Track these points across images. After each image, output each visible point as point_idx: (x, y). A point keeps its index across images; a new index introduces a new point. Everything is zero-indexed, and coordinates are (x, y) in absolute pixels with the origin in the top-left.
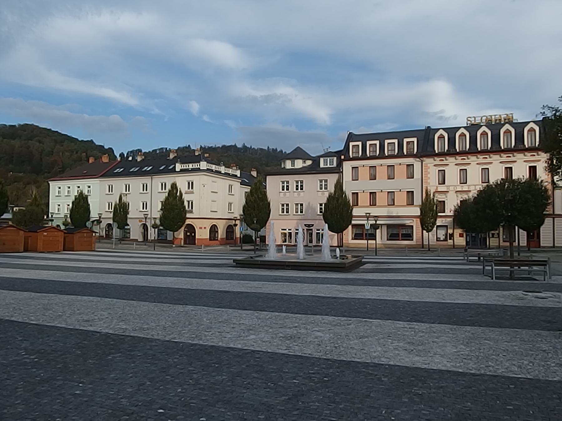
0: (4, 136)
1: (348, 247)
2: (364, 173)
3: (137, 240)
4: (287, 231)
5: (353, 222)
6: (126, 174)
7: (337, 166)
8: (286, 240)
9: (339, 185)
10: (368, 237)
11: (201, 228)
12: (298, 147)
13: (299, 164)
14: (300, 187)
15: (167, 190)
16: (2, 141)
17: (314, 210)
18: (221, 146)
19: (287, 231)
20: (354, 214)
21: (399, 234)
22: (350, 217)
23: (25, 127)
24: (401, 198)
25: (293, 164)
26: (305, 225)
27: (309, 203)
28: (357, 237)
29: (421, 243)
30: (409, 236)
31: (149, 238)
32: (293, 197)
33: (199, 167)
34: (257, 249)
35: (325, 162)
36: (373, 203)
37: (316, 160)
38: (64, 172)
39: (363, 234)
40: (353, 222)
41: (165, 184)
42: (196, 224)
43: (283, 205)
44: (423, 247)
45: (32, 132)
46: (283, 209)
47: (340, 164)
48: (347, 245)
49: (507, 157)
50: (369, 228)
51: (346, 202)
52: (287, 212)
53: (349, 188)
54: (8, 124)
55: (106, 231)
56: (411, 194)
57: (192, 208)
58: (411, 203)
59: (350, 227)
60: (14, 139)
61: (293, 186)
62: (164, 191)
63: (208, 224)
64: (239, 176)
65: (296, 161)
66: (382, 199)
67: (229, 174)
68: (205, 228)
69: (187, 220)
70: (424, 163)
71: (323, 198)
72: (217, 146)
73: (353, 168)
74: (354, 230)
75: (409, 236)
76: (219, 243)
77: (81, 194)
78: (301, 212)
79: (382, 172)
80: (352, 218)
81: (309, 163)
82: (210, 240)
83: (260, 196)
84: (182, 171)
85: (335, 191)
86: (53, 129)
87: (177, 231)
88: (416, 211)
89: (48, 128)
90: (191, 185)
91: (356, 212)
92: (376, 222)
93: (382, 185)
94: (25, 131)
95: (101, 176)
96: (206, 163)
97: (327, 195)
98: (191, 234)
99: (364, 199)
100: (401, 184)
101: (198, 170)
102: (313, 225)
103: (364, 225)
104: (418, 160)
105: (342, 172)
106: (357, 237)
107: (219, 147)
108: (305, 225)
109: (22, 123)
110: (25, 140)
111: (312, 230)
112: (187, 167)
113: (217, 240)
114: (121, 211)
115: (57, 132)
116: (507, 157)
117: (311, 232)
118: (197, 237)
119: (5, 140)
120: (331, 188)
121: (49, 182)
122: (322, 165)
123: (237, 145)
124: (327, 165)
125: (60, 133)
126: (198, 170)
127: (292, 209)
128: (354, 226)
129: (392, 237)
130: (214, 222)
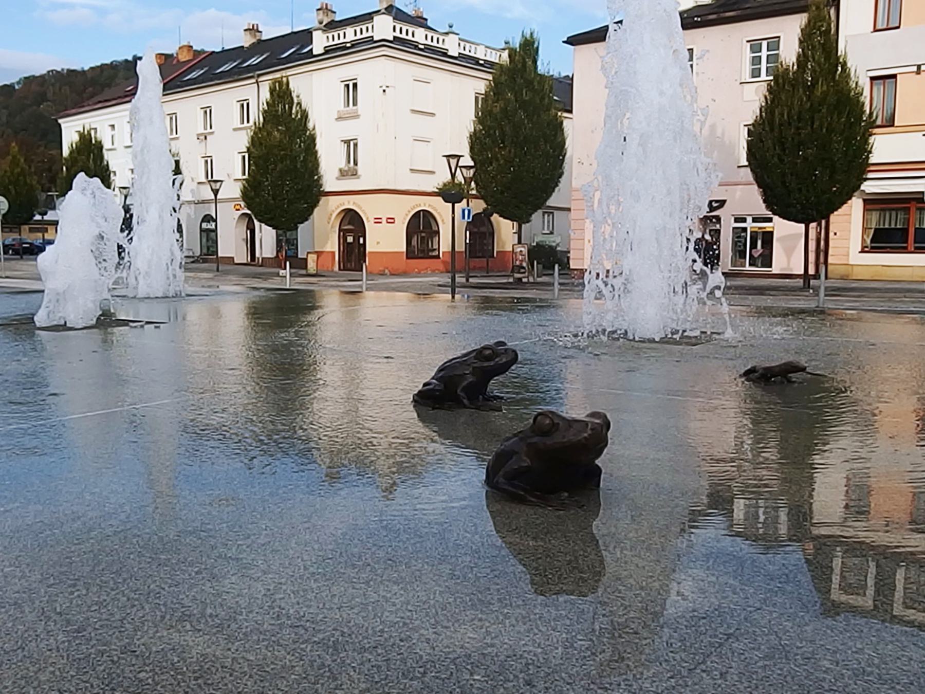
1: (843, 278)
5: (869, 187)
9: (821, 43)
11: (378, 221)
15: (251, 122)
22: (856, 165)
28: (882, 240)
31: (257, 255)
33: (370, 34)
39: (905, 231)
41: (248, 104)
42: (367, 208)
48: (842, 270)
57: (356, 164)
59: (856, 205)
62: (246, 124)
63: (404, 209)
67: (476, 61)
68: (391, 221)
72: (563, 75)
74: (875, 216)
76: (441, 267)
80: (865, 172)
84: (331, 52)
85: (802, 60)
90: (351, 88)
91: (884, 147)
97: (763, 88)
98: (356, 239)
106: (882, 240)
112: (342, 40)
113: (438, 257)
118: (368, 250)
120: (789, 53)
121: (60, 121)
126: (370, 42)
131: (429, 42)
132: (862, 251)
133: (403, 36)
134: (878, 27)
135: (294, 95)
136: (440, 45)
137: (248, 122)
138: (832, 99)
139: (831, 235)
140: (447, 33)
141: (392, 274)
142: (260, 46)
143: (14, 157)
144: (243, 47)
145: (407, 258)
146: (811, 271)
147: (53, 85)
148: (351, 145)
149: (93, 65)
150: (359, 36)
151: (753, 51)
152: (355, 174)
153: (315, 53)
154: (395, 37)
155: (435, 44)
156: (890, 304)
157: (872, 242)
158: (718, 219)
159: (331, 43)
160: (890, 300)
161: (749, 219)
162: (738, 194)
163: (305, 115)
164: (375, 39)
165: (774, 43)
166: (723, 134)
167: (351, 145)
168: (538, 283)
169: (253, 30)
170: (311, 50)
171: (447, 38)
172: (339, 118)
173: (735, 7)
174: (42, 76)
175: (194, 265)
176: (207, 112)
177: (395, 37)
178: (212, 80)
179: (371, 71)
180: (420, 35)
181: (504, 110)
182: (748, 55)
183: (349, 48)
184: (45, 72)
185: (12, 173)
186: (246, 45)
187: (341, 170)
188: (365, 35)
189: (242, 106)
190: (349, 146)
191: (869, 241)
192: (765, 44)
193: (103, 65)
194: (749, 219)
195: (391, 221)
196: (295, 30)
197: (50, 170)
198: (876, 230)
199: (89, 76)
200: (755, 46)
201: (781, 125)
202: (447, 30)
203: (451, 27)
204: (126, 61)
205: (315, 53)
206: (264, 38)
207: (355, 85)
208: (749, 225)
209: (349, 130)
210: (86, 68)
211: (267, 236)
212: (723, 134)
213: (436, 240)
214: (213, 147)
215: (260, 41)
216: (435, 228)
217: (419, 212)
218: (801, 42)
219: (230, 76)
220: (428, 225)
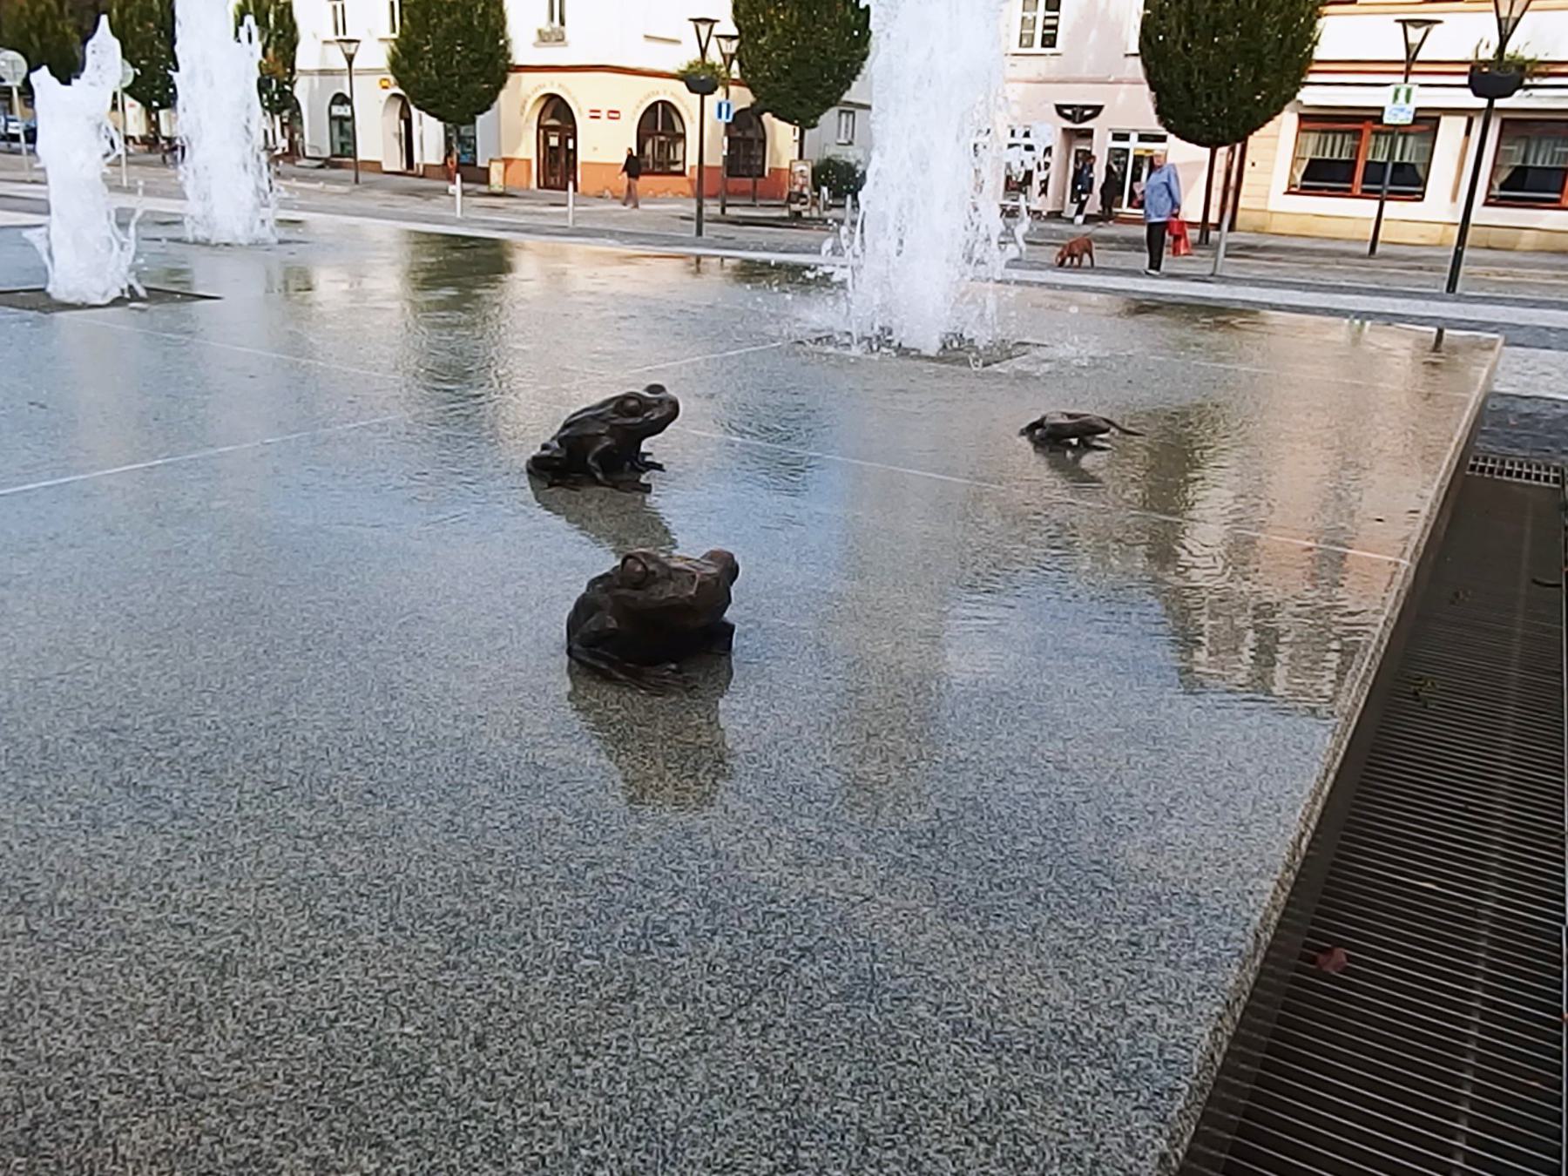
1: (1258, 231)
3: (379, 163)
39: (1352, 164)
42: (579, 93)
48: (1256, 219)
49: (751, 272)
57: (562, 23)
59: (1286, 123)
63: (635, 97)
68: (614, 114)
69: (1308, 89)
74: (1312, 139)
92: (1491, 104)
102: (1098, 109)
106: (1321, 177)
108: (1060, 109)
111: (1089, 134)
113: (682, 173)
116: (751, 272)
128: (1311, 120)
139: (1247, 164)
157: (1304, 178)
158: (1089, 134)
160: (1317, 267)
161: (1134, 137)
162: (1121, 97)
191: (1299, 177)
194: (1134, 137)
195: (614, 114)
198: (1312, 161)
208: (1133, 145)
213: (680, 147)
216: (679, 129)
217: (655, 104)
220: (668, 123)
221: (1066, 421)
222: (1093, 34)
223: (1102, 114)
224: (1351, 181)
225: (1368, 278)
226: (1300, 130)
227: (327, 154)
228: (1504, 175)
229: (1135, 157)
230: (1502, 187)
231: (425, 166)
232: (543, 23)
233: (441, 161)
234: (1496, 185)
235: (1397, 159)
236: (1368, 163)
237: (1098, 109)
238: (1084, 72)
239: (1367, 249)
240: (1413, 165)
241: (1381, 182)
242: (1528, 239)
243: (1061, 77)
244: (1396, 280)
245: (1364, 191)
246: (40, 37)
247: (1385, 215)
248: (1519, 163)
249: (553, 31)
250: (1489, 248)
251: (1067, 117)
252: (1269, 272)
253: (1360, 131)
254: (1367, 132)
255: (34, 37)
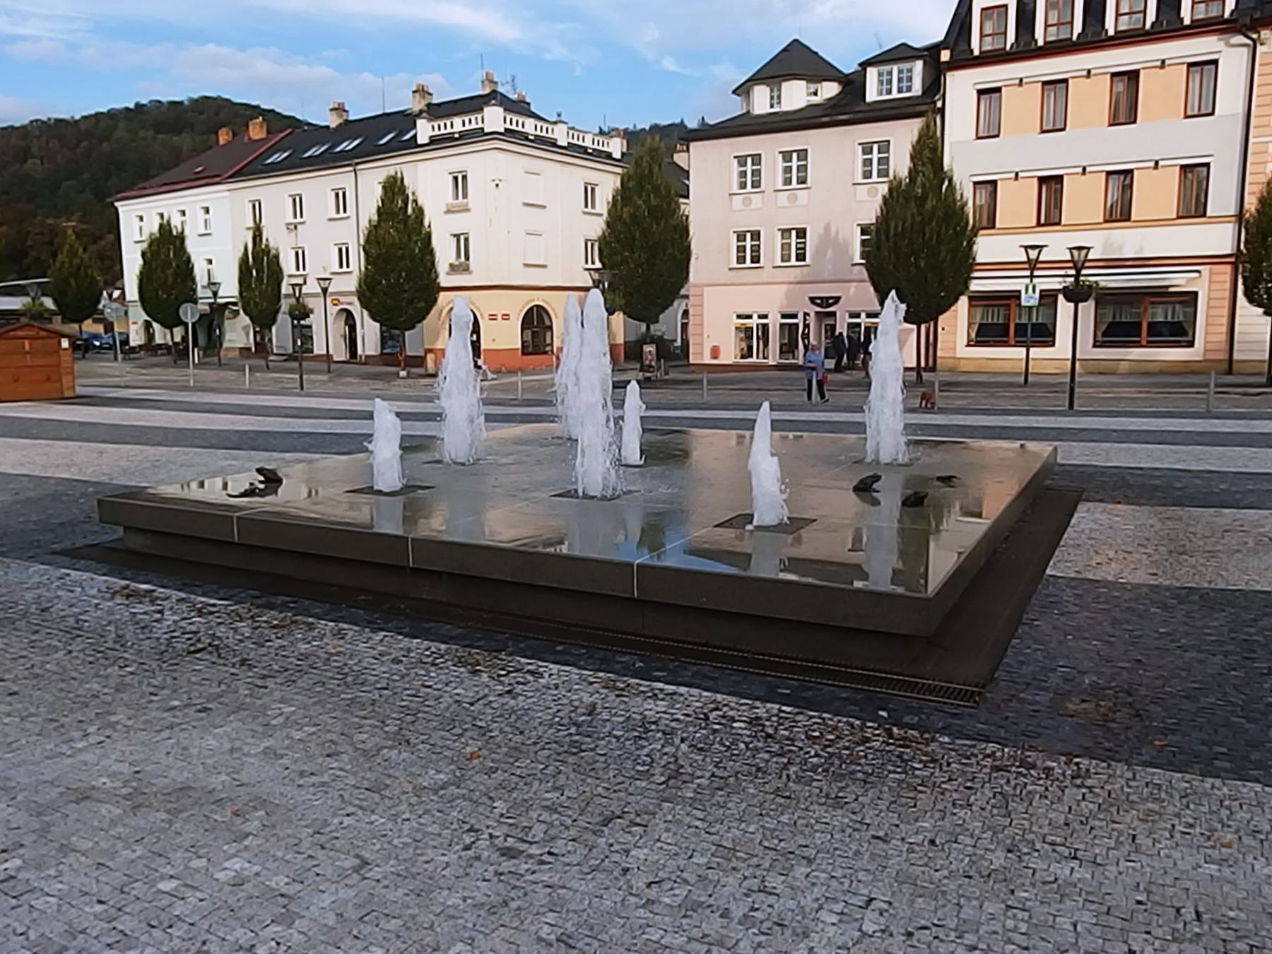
0: (158, 128)
1: (952, 370)
2: (1021, 106)
4: (754, 322)
5: (975, 286)
6: (296, 165)
7: (924, 93)
8: (750, 348)
9: (929, 152)
10: (1029, 338)
11: (493, 317)
12: (796, 41)
13: (796, 95)
14: (798, 171)
16: (154, 138)
17: (844, 248)
18: (647, 128)
19: (754, 322)
20: (979, 260)
21: (1140, 324)
22: (965, 265)
23: (203, 103)
24: (1157, 193)
25: (776, 99)
26: (812, 300)
27: (827, 228)
28: (985, 335)
29: (1225, 356)
30: (1180, 333)
31: (360, 351)
32: (772, 210)
33: (480, 125)
34: (649, 378)
35: (885, 83)
36: (1050, 216)
37: (853, 85)
38: (150, 175)
39: (1007, 326)
40: (975, 286)
43: (741, 237)
44: (1230, 372)
45: (217, 114)
46: (741, 249)
47: (934, 86)
48: (951, 363)
50: (1034, 301)
51: (951, 211)
52: (756, 259)
53: (965, 159)
54: (164, 99)
55: (255, 333)
56: (1194, 177)
57: (467, 258)
58: (1194, 205)
59: (963, 301)
60: (179, 133)
61: (773, 169)
63: (518, 305)
64: (617, 155)
65: (785, 85)
66: (1085, 199)
67: (584, 150)
68: (506, 317)
69: (974, 282)
70: (1259, 48)
71: (868, 204)
72: (639, 127)
73: (981, 92)
74: (979, 311)
75: (1180, 333)
77: (165, 228)
78: (802, 257)
79: (1090, 98)
81: (830, 90)
82: (525, 351)
83: (654, 202)
84: (435, 141)
85: (913, 173)
86: (263, 106)
87: (413, 327)
88: (1220, 238)
89: (254, 103)
90: (460, 182)
91: (987, 248)
93: (1091, 144)
94: (201, 113)
95: (230, 177)
96: (501, 110)
99: (1017, 203)
100: (1163, 136)
101: (478, 135)
102: (837, 299)
103: (1016, 295)
104: (1240, 39)
105: (942, 111)
106: (985, 335)
107: (643, 130)
108: (812, 300)
109: (195, 96)
110: (202, 134)
111: (833, 314)
112: (449, 130)
114: (260, 268)
115: (272, 111)
117: (831, 322)
118: (483, 347)
119: (161, 136)
120: (901, 164)
121: (117, 204)
122: (872, 95)
123: (686, 123)
124: (889, 92)
125: (279, 114)
126: (478, 135)
127: (771, 247)
129: (1115, 332)
130: (538, 298)
131: (538, 133)
132: (968, 345)
133: (514, 127)
134: (981, 134)
135: (409, 192)
136: (550, 135)
137: (345, 211)
138: (940, 213)
139: (940, 329)
140: (555, 123)
141: (509, 372)
142: (349, 128)
143: (71, 246)
144: (328, 127)
145: (523, 354)
146: (923, 364)
147: (38, 137)
148: (462, 242)
149: (85, 114)
150: (468, 127)
151: (864, 153)
152: (465, 269)
153: (420, 142)
154: (506, 130)
155: (544, 134)
156: (993, 401)
157: (977, 335)
158: (833, 314)
159: (436, 132)
160: (993, 395)
161: (863, 315)
162: (852, 291)
163: (420, 212)
164: (486, 130)
165: (884, 146)
166: (837, 232)
167: (462, 242)
168: (666, 381)
169: (339, 109)
170: (415, 136)
171: (556, 128)
172: (448, 212)
173: (847, 110)
174: (23, 127)
175: (287, 365)
176: (297, 202)
177: (506, 130)
178: (302, 166)
179: (482, 164)
180: (529, 126)
181: (633, 216)
182: (860, 157)
183: (457, 139)
184: (26, 122)
185: (71, 263)
186: (333, 125)
187: (451, 265)
188: (474, 126)
189: (337, 195)
190: (458, 241)
191: (973, 335)
192: (875, 147)
193: (98, 114)
194: (863, 315)
195: (506, 317)
196: (388, 111)
197: (51, 243)
198: (980, 325)
199: (83, 127)
200: (867, 149)
201: (895, 235)
202: (554, 119)
203: (559, 115)
204: (127, 109)
205: (420, 142)
206: (352, 118)
207: (464, 177)
208: (863, 320)
209: (459, 223)
210: (77, 117)
211: (369, 334)
212: (837, 232)
213: (548, 334)
214: (304, 237)
215: (347, 122)
216: (547, 323)
217: (532, 308)
218: (912, 158)
219: (323, 163)
220: (541, 319)
221: (426, 224)
222: (830, 252)
223: (841, 301)
224: (1139, 336)
225: (1025, 402)
226: (970, 306)
227: (291, 351)
228: (1104, 327)
229: (866, 328)
230: (1104, 335)
231: (367, 357)
232: (453, 260)
233: (379, 352)
234: (1099, 334)
235: (1034, 321)
236: (1017, 325)
237: (837, 299)
238: (826, 276)
239: (1022, 379)
240: (1044, 325)
241: (1026, 336)
242: (1124, 365)
243: (811, 279)
244: (1043, 401)
245: (1149, 342)
246: (76, 281)
247: (1031, 356)
248: (1110, 320)
249: (461, 264)
250: (1101, 373)
251: (818, 305)
252: (965, 402)
253: (1009, 305)
254: (1013, 306)
255: (72, 282)
